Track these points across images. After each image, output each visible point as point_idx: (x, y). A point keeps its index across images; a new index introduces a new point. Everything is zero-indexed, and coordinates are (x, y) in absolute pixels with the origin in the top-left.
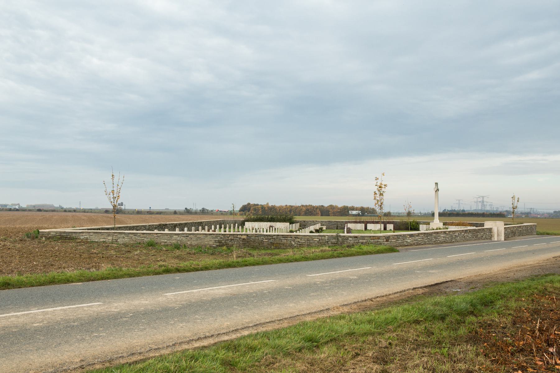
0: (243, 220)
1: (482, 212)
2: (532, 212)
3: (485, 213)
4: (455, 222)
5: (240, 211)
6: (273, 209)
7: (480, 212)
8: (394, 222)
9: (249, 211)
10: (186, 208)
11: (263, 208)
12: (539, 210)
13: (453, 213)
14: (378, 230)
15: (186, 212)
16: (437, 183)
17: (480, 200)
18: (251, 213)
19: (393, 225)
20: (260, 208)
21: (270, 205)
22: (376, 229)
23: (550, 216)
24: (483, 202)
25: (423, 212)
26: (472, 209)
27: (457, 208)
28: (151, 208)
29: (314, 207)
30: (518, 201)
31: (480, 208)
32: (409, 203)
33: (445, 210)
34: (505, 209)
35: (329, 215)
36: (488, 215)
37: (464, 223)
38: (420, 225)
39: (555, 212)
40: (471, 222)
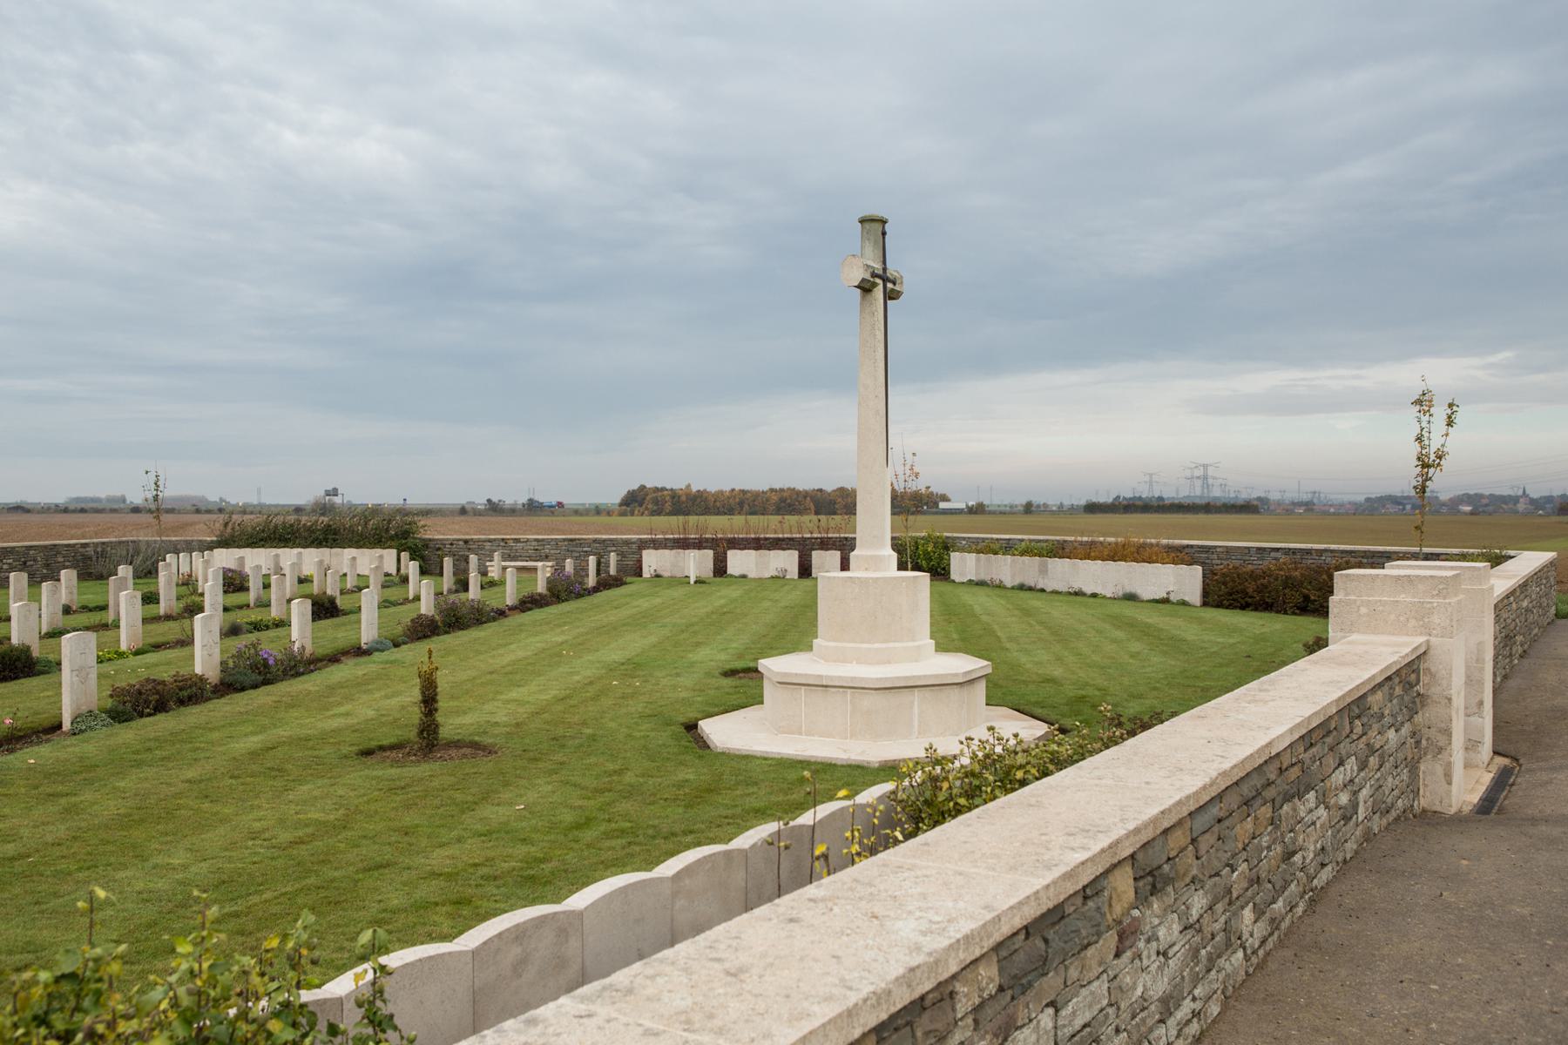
0: (215, 539)
1: (1203, 502)
2: (1315, 501)
3: (1212, 504)
4: (1102, 539)
5: (621, 505)
6: (699, 500)
7: (1198, 501)
8: (846, 539)
9: (641, 505)
10: (489, 501)
11: (676, 498)
12: (1332, 497)
13: (1134, 505)
14: (772, 577)
15: (489, 509)
16: (884, 222)
18: (647, 509)
19: (814, 553)
20: (668, 498)
21: (694, 489)
22: (767, 575)
23: (1356, 509)
24: (1205, 477)
25: (1067, 503)
26: (1181, 495)
28: (408, 502)
29: (798, 493)
30: (1450, 423)
31: (1198, 492)
32: (909, 457)
33: (1118, 497)
34: (1255, 495)
36: (1220, 507)
37: (1143, 546)
39: (1368, 500)
40: (1177, 542)
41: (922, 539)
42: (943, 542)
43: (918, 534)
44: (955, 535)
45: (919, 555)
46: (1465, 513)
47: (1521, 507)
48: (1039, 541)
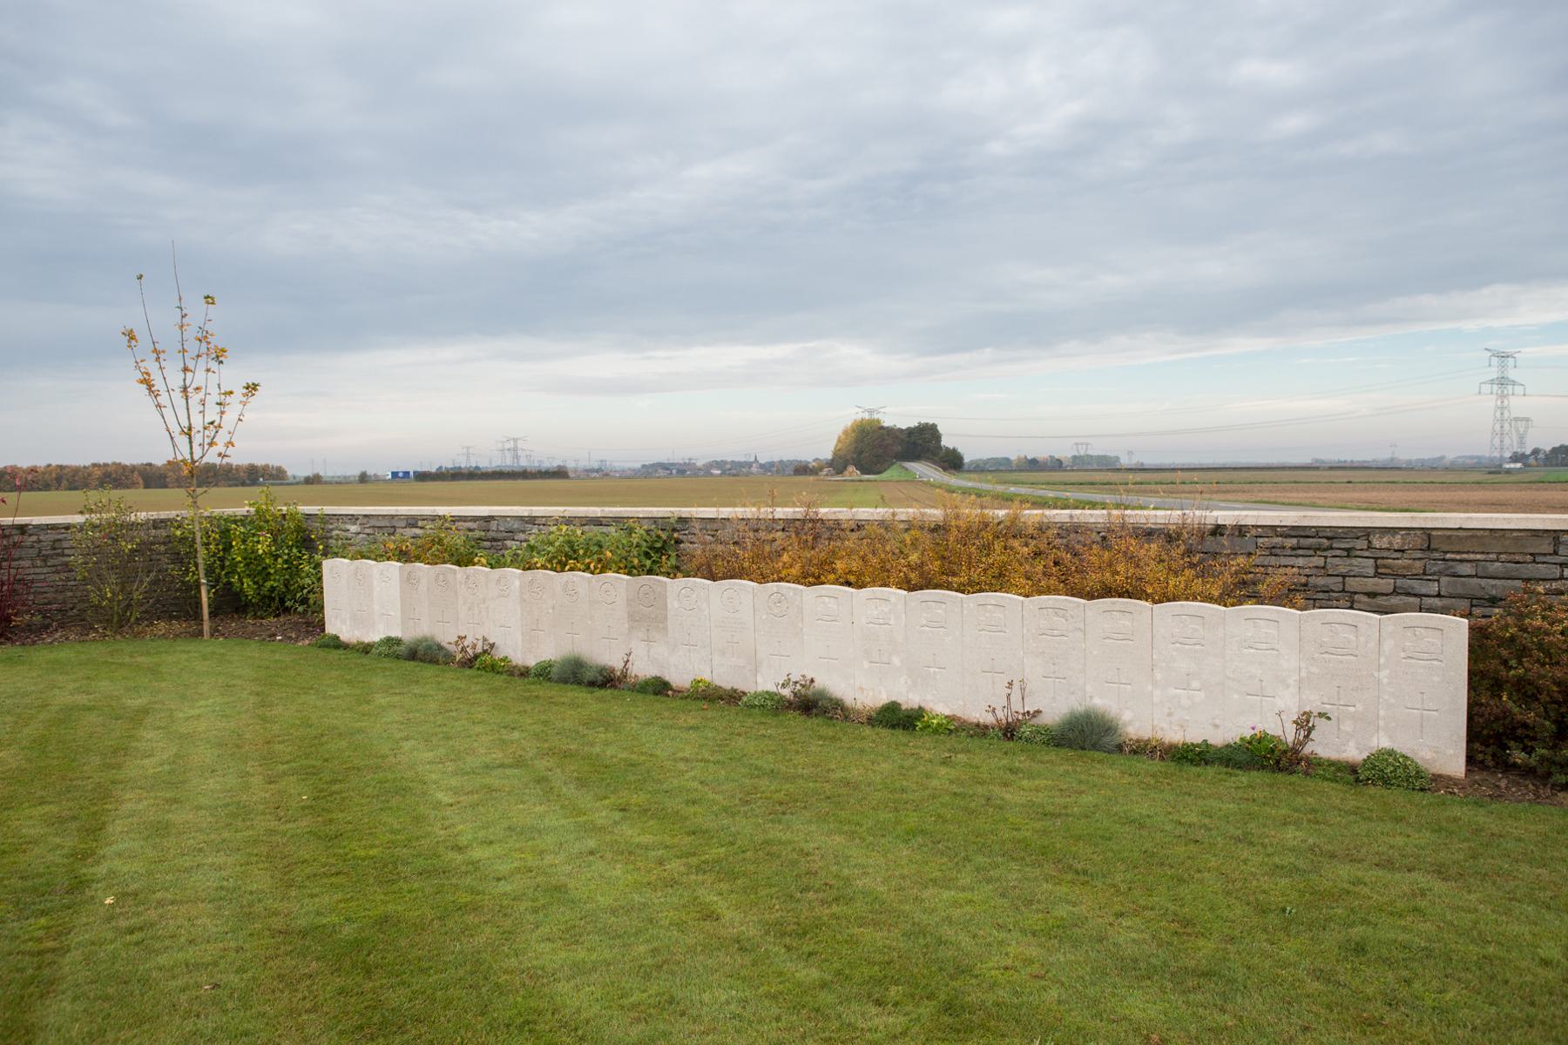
3: (529, 470)
8: (22, 529)
12: (616, 464)
17: (511, 445)
24: (515, 449)
26: (493, 465)
27: (463, 463)
29: (124, 467)
33: (441, 467)
35: (166, 486)
36: (535, 474)
38: (328, 565)
39: (644, 466)
41: (242, 521)
42: (299, 529)
43: (229, 511)
44: (329, 510)
45: (235, 565)
46: (717, 476)
47: (754, 469)
48: (597, 522)
